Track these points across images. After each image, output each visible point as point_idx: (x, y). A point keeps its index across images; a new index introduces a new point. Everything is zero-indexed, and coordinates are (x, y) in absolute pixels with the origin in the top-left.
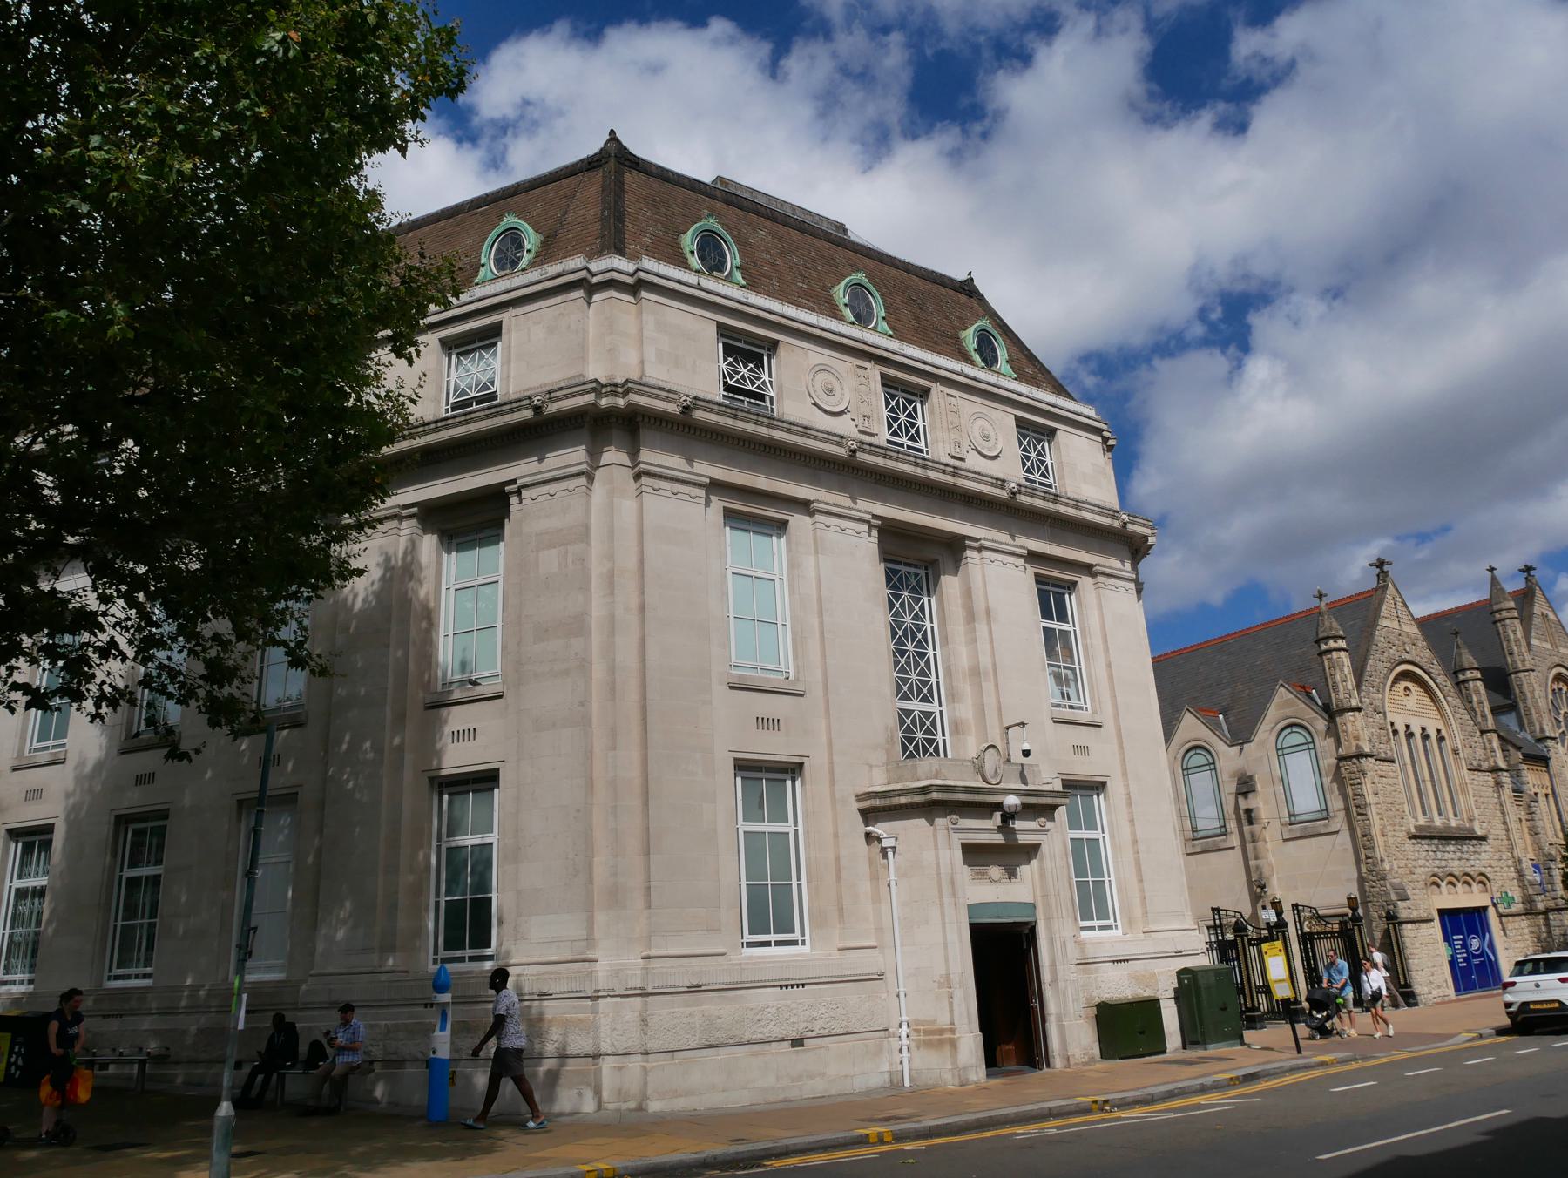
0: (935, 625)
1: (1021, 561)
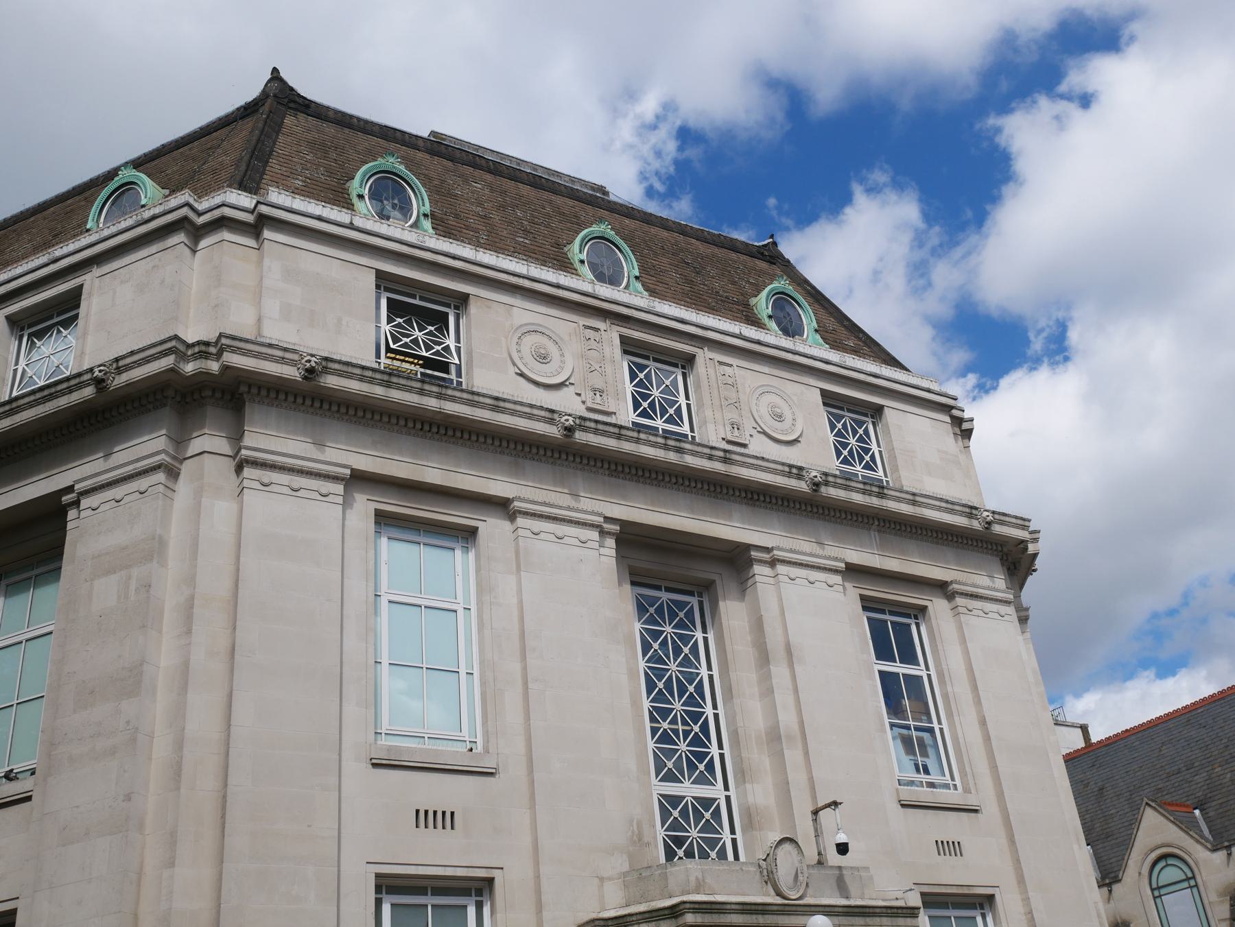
0: (715, 673)
1: (837, 579)
